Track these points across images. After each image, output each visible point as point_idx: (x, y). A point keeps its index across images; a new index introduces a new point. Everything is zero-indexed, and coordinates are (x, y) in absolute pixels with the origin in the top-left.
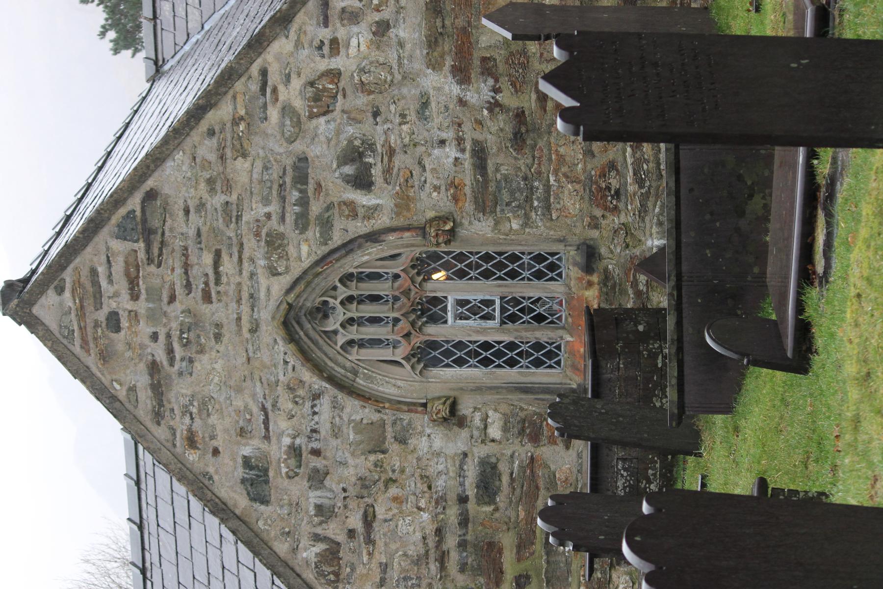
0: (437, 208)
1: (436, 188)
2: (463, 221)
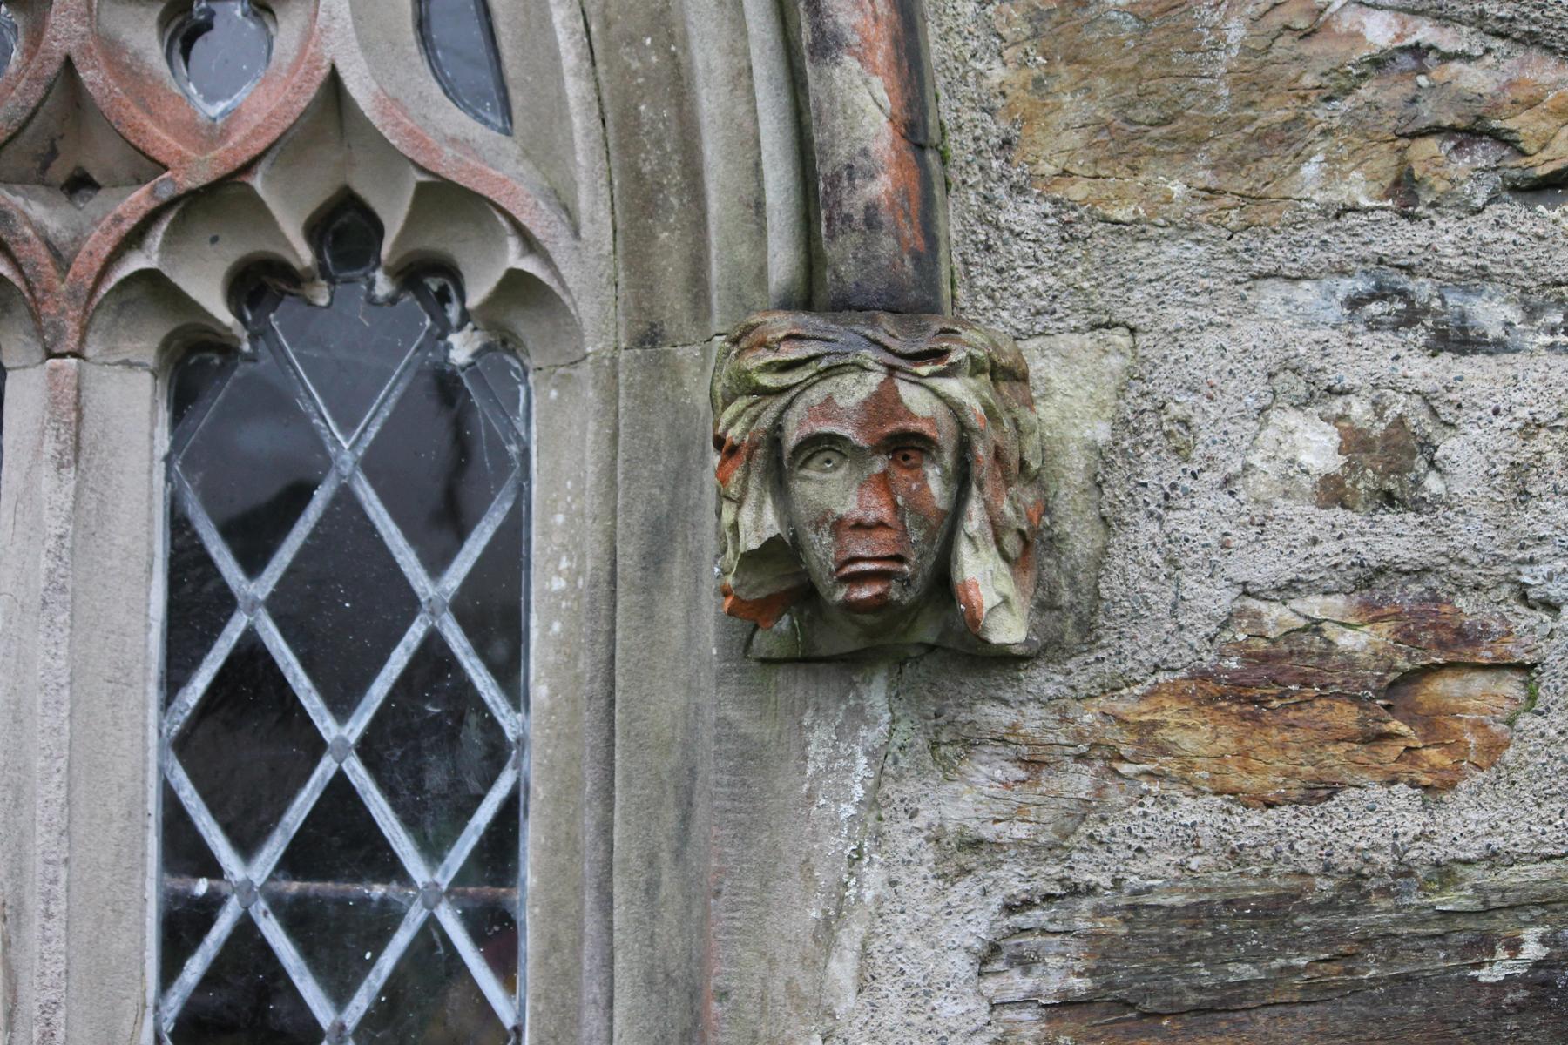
0: (1157, 470)
1: (1387, 467)
2: (988, 773)
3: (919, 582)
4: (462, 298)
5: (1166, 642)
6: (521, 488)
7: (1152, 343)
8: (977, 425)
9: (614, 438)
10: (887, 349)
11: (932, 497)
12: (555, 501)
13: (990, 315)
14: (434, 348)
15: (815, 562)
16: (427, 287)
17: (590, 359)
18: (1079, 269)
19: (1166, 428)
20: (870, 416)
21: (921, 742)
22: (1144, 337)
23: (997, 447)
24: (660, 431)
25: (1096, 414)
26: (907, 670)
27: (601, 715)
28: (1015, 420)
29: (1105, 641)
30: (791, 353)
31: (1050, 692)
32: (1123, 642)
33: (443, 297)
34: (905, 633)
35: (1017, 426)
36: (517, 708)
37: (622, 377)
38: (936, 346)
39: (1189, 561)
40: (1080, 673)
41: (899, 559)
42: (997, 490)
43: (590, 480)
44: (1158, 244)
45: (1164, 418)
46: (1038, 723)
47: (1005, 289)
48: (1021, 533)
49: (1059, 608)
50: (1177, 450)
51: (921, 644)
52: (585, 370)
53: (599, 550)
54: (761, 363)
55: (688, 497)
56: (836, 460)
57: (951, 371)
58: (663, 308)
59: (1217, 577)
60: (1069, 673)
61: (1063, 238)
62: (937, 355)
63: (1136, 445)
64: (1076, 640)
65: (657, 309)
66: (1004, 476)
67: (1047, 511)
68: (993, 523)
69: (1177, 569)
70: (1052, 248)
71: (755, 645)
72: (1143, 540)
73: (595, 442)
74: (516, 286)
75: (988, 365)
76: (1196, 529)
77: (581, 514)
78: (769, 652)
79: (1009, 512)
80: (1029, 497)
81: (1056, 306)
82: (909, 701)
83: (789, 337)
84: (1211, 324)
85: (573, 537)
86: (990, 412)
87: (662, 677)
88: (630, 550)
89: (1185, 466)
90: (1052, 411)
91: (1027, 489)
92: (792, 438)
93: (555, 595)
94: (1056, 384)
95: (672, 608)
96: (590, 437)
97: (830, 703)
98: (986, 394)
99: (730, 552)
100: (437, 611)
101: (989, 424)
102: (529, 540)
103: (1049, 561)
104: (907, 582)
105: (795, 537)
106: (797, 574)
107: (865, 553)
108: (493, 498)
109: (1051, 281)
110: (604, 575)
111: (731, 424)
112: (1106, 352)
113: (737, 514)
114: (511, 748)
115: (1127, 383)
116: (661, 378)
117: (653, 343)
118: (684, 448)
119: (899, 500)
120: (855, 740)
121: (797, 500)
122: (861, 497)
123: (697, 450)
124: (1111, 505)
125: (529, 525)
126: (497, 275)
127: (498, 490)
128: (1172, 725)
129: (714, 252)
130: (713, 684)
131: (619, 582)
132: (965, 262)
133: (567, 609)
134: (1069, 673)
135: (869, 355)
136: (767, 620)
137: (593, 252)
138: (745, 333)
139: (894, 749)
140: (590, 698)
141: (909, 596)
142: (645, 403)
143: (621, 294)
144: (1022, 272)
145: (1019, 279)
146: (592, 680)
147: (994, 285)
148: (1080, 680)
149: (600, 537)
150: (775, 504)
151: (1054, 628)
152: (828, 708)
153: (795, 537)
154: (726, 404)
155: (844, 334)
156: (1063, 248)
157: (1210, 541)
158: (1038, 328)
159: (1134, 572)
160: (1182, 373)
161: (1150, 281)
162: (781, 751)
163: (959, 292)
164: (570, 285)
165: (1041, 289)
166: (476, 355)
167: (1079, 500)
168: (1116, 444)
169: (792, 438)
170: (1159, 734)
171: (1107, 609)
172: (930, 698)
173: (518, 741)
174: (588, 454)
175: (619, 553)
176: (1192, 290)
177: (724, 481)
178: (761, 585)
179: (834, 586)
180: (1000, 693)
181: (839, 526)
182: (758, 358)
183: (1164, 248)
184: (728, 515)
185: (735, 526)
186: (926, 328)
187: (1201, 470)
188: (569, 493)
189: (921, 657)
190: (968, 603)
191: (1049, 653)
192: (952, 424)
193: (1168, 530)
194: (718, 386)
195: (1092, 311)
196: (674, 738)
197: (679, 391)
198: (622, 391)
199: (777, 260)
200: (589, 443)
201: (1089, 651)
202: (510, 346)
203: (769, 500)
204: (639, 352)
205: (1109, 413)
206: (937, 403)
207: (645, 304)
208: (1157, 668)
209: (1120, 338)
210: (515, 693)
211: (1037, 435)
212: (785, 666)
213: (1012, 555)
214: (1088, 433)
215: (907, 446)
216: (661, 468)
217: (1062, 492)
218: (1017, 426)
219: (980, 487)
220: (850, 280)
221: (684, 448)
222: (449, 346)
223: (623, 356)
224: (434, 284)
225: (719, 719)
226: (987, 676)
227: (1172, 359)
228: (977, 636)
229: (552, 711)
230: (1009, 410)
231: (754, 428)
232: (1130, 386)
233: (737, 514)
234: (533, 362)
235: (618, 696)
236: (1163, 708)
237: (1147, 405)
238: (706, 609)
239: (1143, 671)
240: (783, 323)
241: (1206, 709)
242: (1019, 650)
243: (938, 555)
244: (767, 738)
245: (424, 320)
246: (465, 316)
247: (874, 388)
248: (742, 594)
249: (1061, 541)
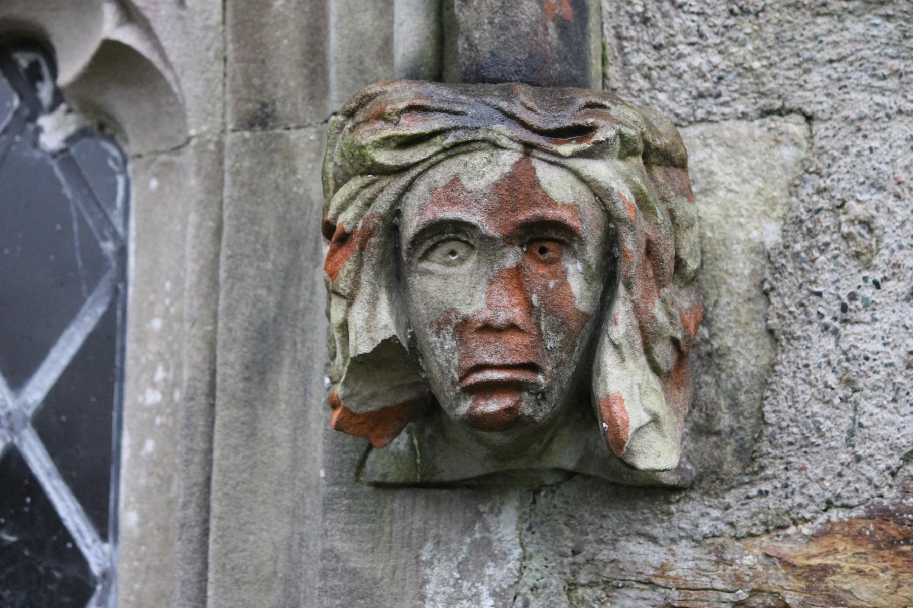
0: (834, 278)
3: (555, 395)
4: (54, 73)
5: (840, 475)
6: (116, 291)
7: (831, 133)
8: (627, 214)
9: (218, 232)
10: (524, 124)
11: (572, 296)
12: (152, 304)
13: (646, 97)
14: (22, 132)
15: (435, 370)
16: (15, 64)
17: (193, 142)
18: (750, 47)
19: (845, 229)
20: (502, 201)
21: (556, 582)
22: (822, 126)
23: (649, 242)
24: (269, 226)
25: (765, 213)
26: (542, 500)
27: (194, 545)
28: (671, 212)
29: (769, 472)
30: (413, 126)
31: (705, 529)
32: (790, 474)
33: (34, 75)
34: (539, 456)
35: (673, 218)
36: (104, 537)
37: (228, 163)
38: (581, 122)
39: (869, 382)
40: (741, 507)
41: (533, 368)
42: (647, 292)
43: (190, 279)
44: (841, 20)
45: (843, 218)
46: (691, 564)
47: (663, 68)
48: (675, 342)
49: (718, 433)
50: (857, 255)
51: (558, 470)
52: (188, 157)
53: (198, 358)
54: (378, 137)
55: (298, 298)
56: (462, 251)
57: (596, 152)
58: (276, 85)
59: (902, 402)
60: (728, 507)
61: (732, 12)
62: (581, 132)
63: (809, 249)
64: (736, 470)
65: (269, 86)
66: (656, 275)
67: (705, 320)
68: (642, 329)
69: (855, 391)
70: (718, 22)
71: (368, 467)
72: (815, 357)
73: (196, 236)
74: (113, 60)
75: (640, 146)
76: (879, 347)
77: (179, 318)
78: (385, 475)
79: (661, 317)
80: (685, 301)
81: (722, 88)
82: (543, 535)
83: (411, 109)
84: (900, 112)
85: (170, 344)
86: (642, 201)
87: (264, 502)
88: (232, 357)
89: (866, 273)
90: (714, 209)
91: (683, 293)
92: (412, 224)
93: (149, 409)
94: (720, 177)
95: (277, 425)
96: (191, 230)
97: (453, 535)
98: (637, 180)
99: (339, 357)
100: (16, 427)
101: (640, 215)
102: (123, 349)
103: (707, 378)
104: (541, 395)
105: (414, 340)
106: (417, 384)
107: (494, 360)
108: (83, 301)
109: (716, 59)
110: (202, 386)
111: (343, 208)
112: (778, 142)
113: (347, 312)
114: (96, 583)
115: (801, 178)
116: (272, 164)
117: (264, 125)
118: (296, 244)
119: (534, 299)
120: (480, 579)
121: (416, 297)
122: (489, 294)
123: (310, 245)
124: (779, 316)
125: (124, 332)
126: (91, 48)
127: (90, 292)
128: (846, 570)
129: (333, 19)
130: (319, 510)
131: (218, 394)
132: (619, 37)
133: (163, 425)
134: (728, 507)
135: (502, 131)
136: (381, 437)
137: (199, 22)
138: (361, 105)
139: (525, 590)
140: (182, 526)
141: (543, 412)
142: (253, 192)
143: (229, 69)
144: (684, 49)
145: (680, 56)
146: (185, 506)
147: (651, 63)
148: (740, 515)
149: (199, 343)
150: (391, 302)
151: (712, 456)
152: (450, 541)
153: (414, 340)
154: (338, 187)
155: (474, 107)
156: (731, 22)
157: (894, 360)
158: (700, 114)
159: (805, 393)
160: (866, 167)
161: (831, 61)
162: (394, 590)
163: (612, 71)
164: (172, 58)
165: (705, 68)
166: (71, 140)
167: (743, 310)
168: (787, 247)
169: (412, 224)
170: (831, 581)
171: (773, 435)
172: (567, 532)
173: (105, 575)
174: (188, 249)
175: (219, 361)
176: (879, 73)
177: (333, 274)
178: (373, 396)
179: (457, 399)
180: (648, 529)
181: (463, 328)
182: (375, 131)
183: (848, 23)
184: (337, 315)
185: (344, 327)
186: (570, 102)
187: (885, 279)
188: (168, 295)
189: (558, 485)
190: (612, 422)
191: (704, 484)
192: (591, 195)
193: (845, 346)
194: (330, 166)
195: (763, 94)
196: (275, 573)
197: (292, 179)
198: (227, 178)
199: (404, 29)
200: (189, 237)
201: (751, 483)
202: (108, 131)
203: (384, 297)
204: (247, 134)
205: (779, 211)
206: (580, 188)
207: (256, 81)
208: (829, 504)
209: (794, 126)
210: (102, 518)
211: (696, 229)
212: (403, 492)
213: (664, 367)
214: (755, 234)
215: (544, 237)
216: (269, 266)
217: (723, 301)
218: (673, 218)
219: (628, 286)
220: (485, 49)
221: (296, 244)
222: (38, 130)
223: (229, 138)
224: (24, 60)
225: (325, 551)
226: (633, 509)
227: (854, 151)
228: (622, 460)
229: (141, 541)
230: (664, 199)
231: (368, 213)
232: (805, 181)
233: (347, 312)
234: (132, 148)
235: (213, 523)
236: (836, 551)
237: (824, 203)
238: (313, 425)
239: (813, 507)
240: (405, 93)
241: (886, 553)
242: (670, 479)
243: (578, 365)
244: (379, 574)
245: (11, 100)
246: (58, 96)
247: (507, 169)
248: (352, 405)
249: (721, 356)
